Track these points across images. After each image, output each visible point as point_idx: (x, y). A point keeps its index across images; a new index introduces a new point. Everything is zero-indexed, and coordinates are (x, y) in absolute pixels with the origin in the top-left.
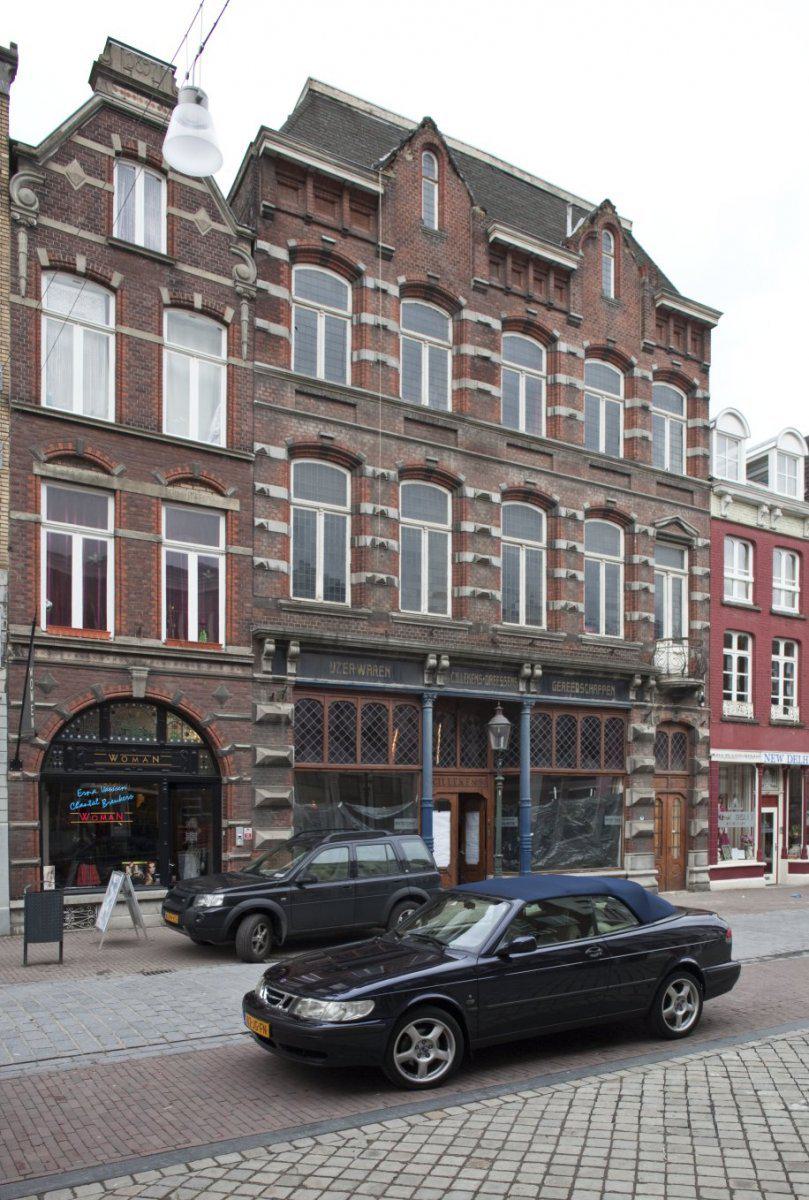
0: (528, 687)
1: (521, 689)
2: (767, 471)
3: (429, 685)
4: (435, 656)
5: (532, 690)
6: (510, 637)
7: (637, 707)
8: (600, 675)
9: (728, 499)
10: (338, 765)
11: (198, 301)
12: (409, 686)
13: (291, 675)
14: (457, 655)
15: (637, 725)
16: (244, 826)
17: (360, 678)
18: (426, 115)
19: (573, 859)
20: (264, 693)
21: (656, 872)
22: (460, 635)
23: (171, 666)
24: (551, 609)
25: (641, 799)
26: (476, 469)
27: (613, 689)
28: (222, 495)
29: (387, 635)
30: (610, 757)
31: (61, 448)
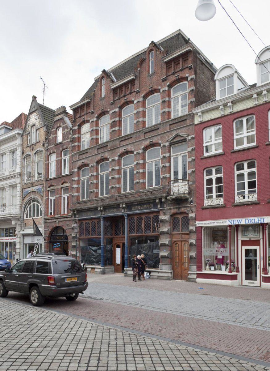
0: (124, 210)
2: (233, 86)
6: (120, 197)
8: (146, 202)
10: (87, 237)
12: (97, 216)
15: (162, 217)
18: (153, 40)
23: (62, 220)
24: (98, 190)
26: (112, 153)
27: (152, 205)
29: (93, 204)
30: (184, 226)
31: (63, 181)
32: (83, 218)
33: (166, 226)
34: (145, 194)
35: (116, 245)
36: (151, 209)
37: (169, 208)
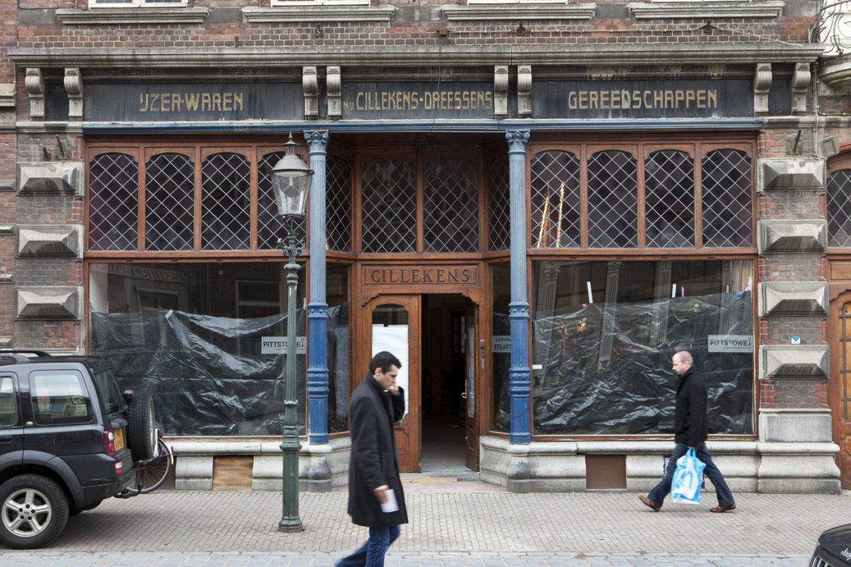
1: (498, 111)
3: (314, 117)
4: (314, 69)
5: (521, 111)
7: (772, 125)
8: (676, 72)
10: (218, 252)
12: (276, 122)
13: (76, 118)
14: (355, 63)
17: (189, 115)
19: (636, 414)
20: (35, 148)
21: (835, 447)
22: (374, 31)
25: (783, 302)
32: (137, 124)
33: (804, 211)
34: (658, 26)
35: (372, 307)
36: (702, 113)
37: (823, 119)
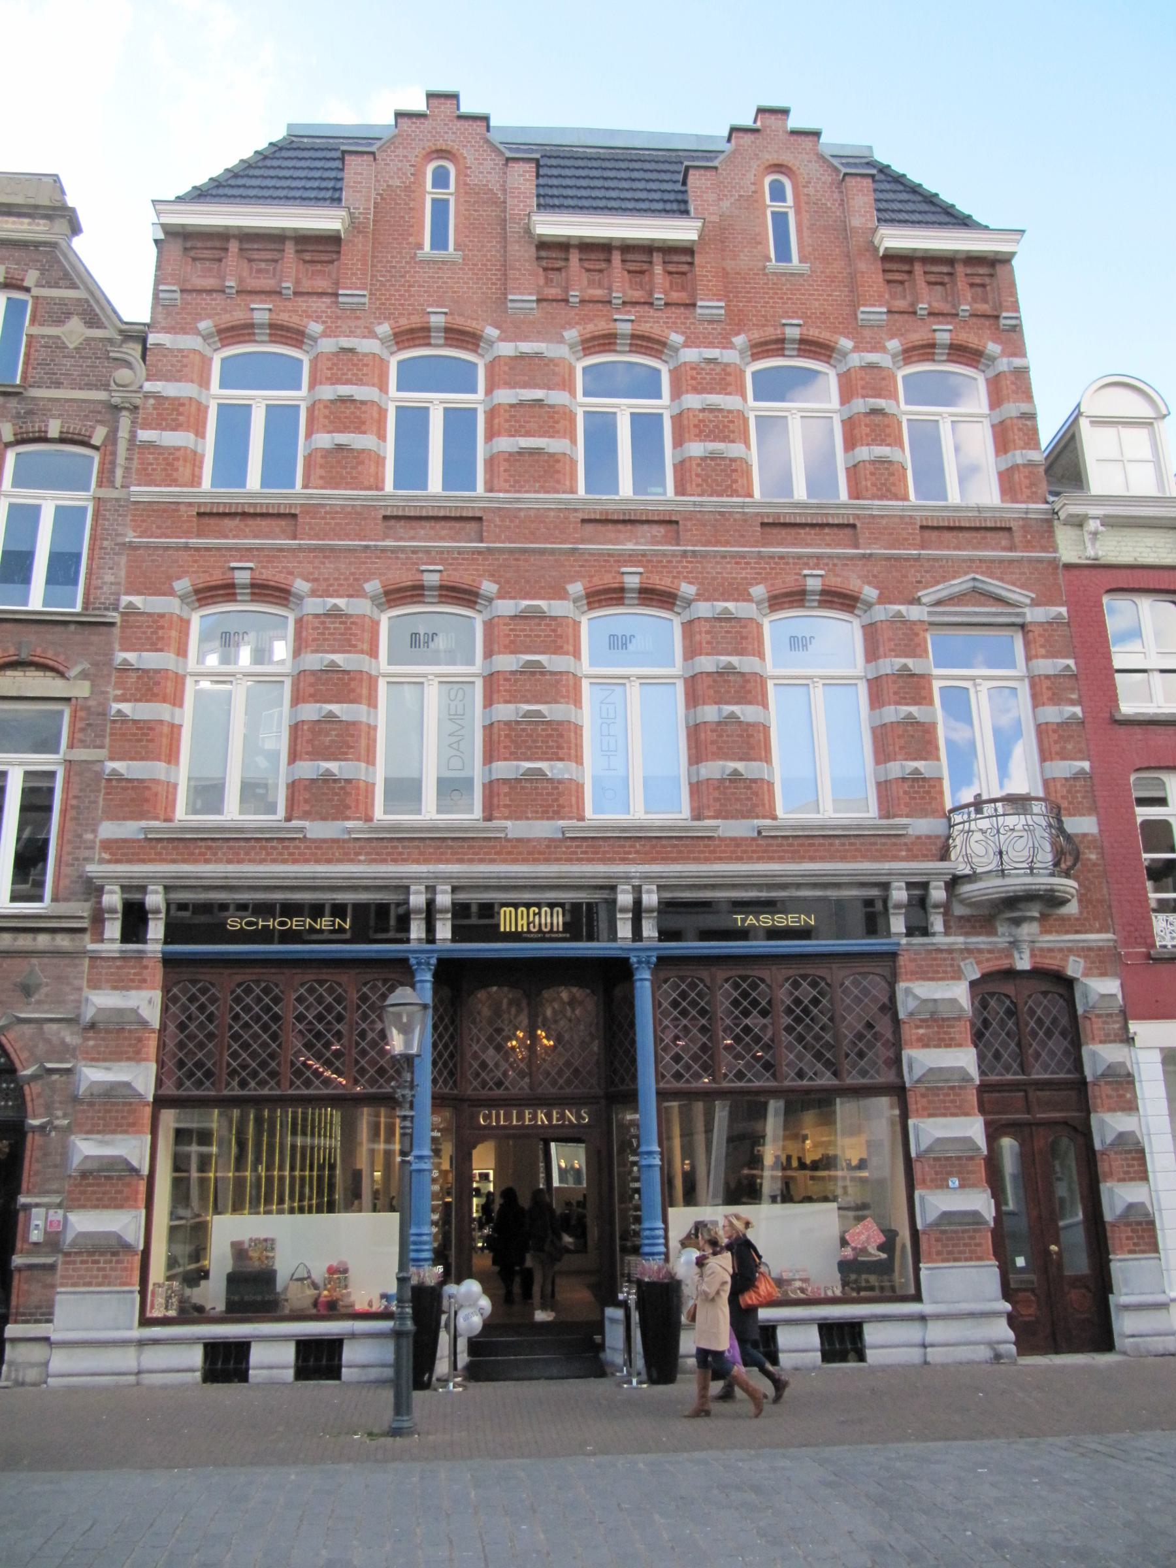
9: (1093, 525)
11: (54, 431)
16: (48, 1206)
28: (62, 675)
